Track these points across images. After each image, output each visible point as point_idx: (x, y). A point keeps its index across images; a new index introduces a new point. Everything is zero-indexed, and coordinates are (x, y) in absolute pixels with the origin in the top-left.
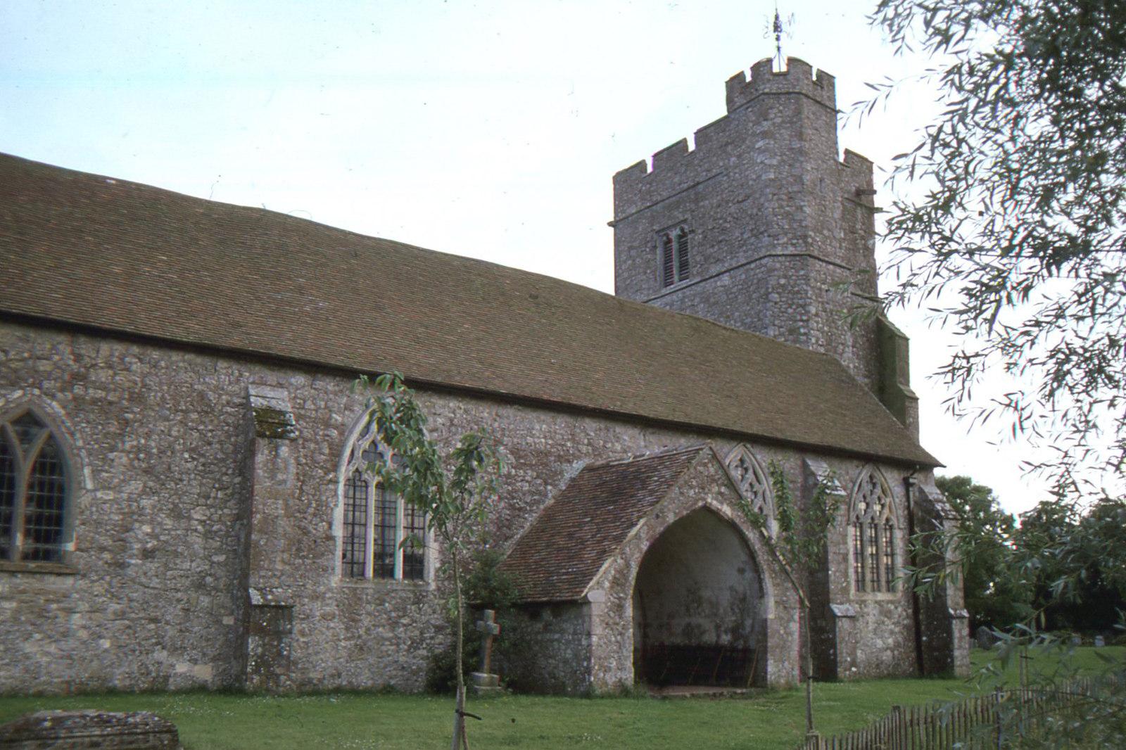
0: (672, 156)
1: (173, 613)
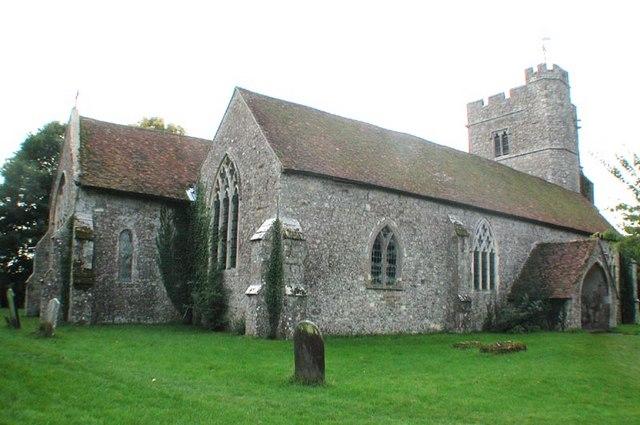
0: (497, 99)
1: (429, 305)
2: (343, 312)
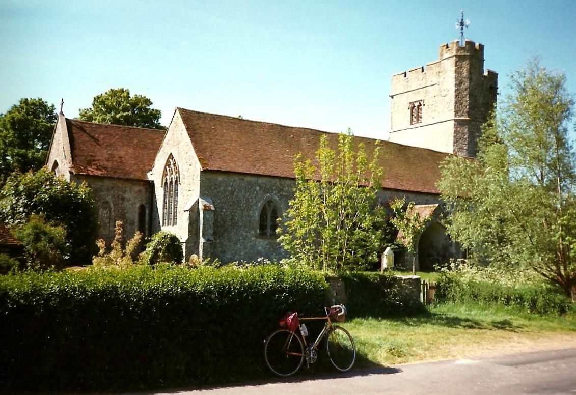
2: (240, 252)
